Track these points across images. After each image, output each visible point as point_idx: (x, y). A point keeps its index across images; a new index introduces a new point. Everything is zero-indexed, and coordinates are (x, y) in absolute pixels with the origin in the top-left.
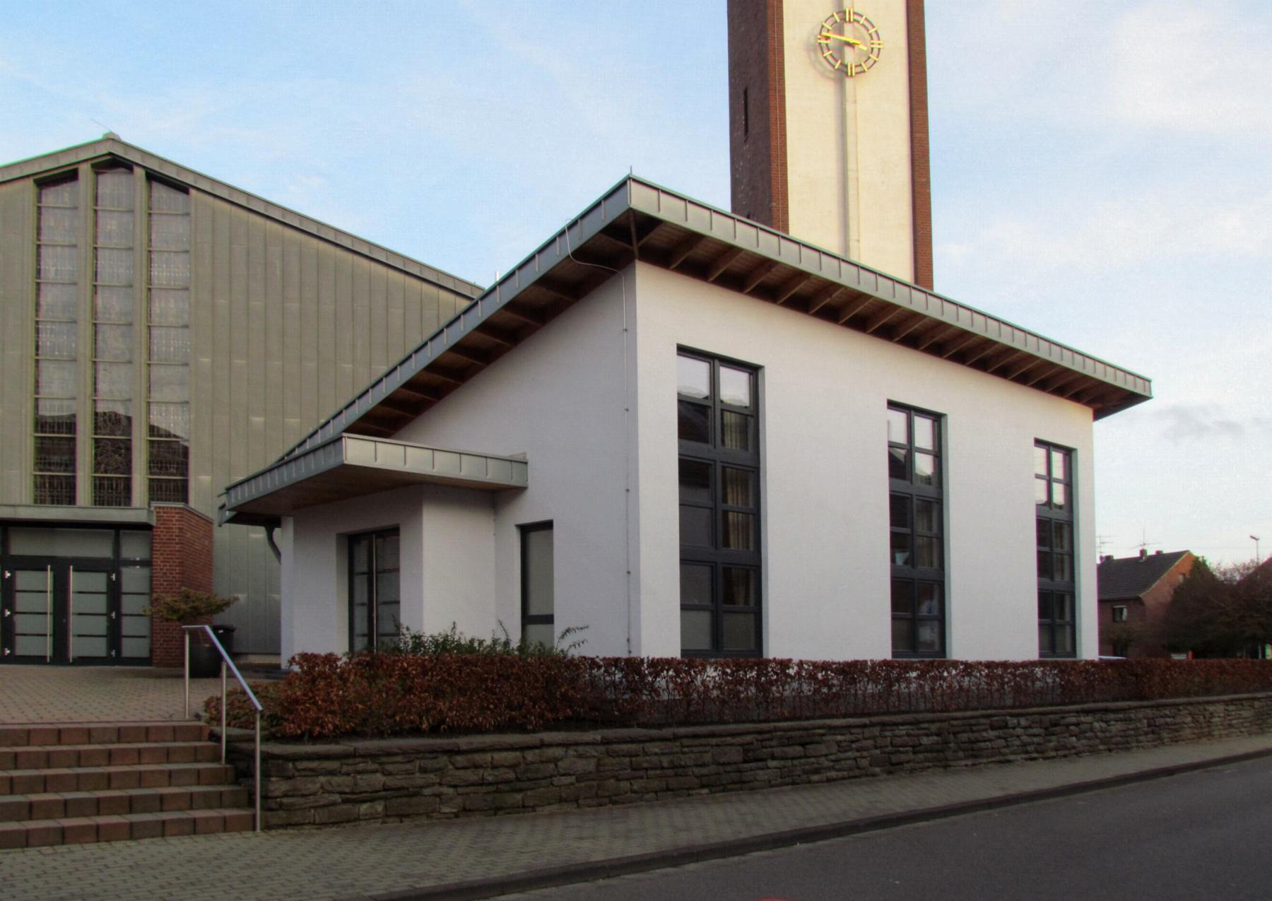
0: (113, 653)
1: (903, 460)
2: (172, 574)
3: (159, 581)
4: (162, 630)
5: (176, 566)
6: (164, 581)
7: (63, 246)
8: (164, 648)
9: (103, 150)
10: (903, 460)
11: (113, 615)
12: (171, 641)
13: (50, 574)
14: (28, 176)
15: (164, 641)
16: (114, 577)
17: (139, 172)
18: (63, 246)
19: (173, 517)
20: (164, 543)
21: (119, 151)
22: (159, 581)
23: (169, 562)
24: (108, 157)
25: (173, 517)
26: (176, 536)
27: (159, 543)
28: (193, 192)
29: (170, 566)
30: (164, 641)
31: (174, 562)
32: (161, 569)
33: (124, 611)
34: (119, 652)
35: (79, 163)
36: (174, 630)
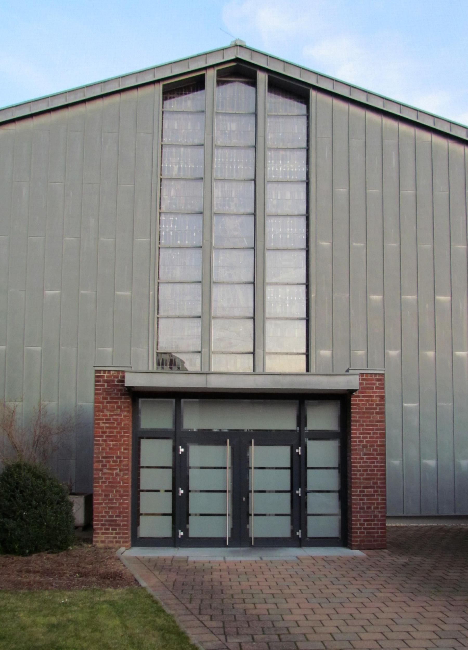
0: (299, 533)
1: (138, 537)
2: (372, 446)
3: (359, 454)
4: (363, 508)
5: (377, 438)
6: (365, 454)
7: (186, 146)
8: (365, 529)
9: (230, 56)
10: (138, 537)
11: (299, 492)
12: (373, 520)
13: (228, 447)
14: (158, 81)
15: (364, 520)
16: (299, 451)
17: (262, 78)
18: (186, 146)
19: (374, 384)
20: (364, 413)
21: (245, 57)
22: (359, 454)
23: (369, 434)
24: (233, 64)
25: (374, 384)
26: (377, 405)
27: (358, 413)
28: (313, 94)
29: (370, 438)
30: (364, 520)
31: (374, 433)
32: (360, 442)
33: (289, 495)
34: (305, 533)
35: (205, 68)
36: (376, 508)
